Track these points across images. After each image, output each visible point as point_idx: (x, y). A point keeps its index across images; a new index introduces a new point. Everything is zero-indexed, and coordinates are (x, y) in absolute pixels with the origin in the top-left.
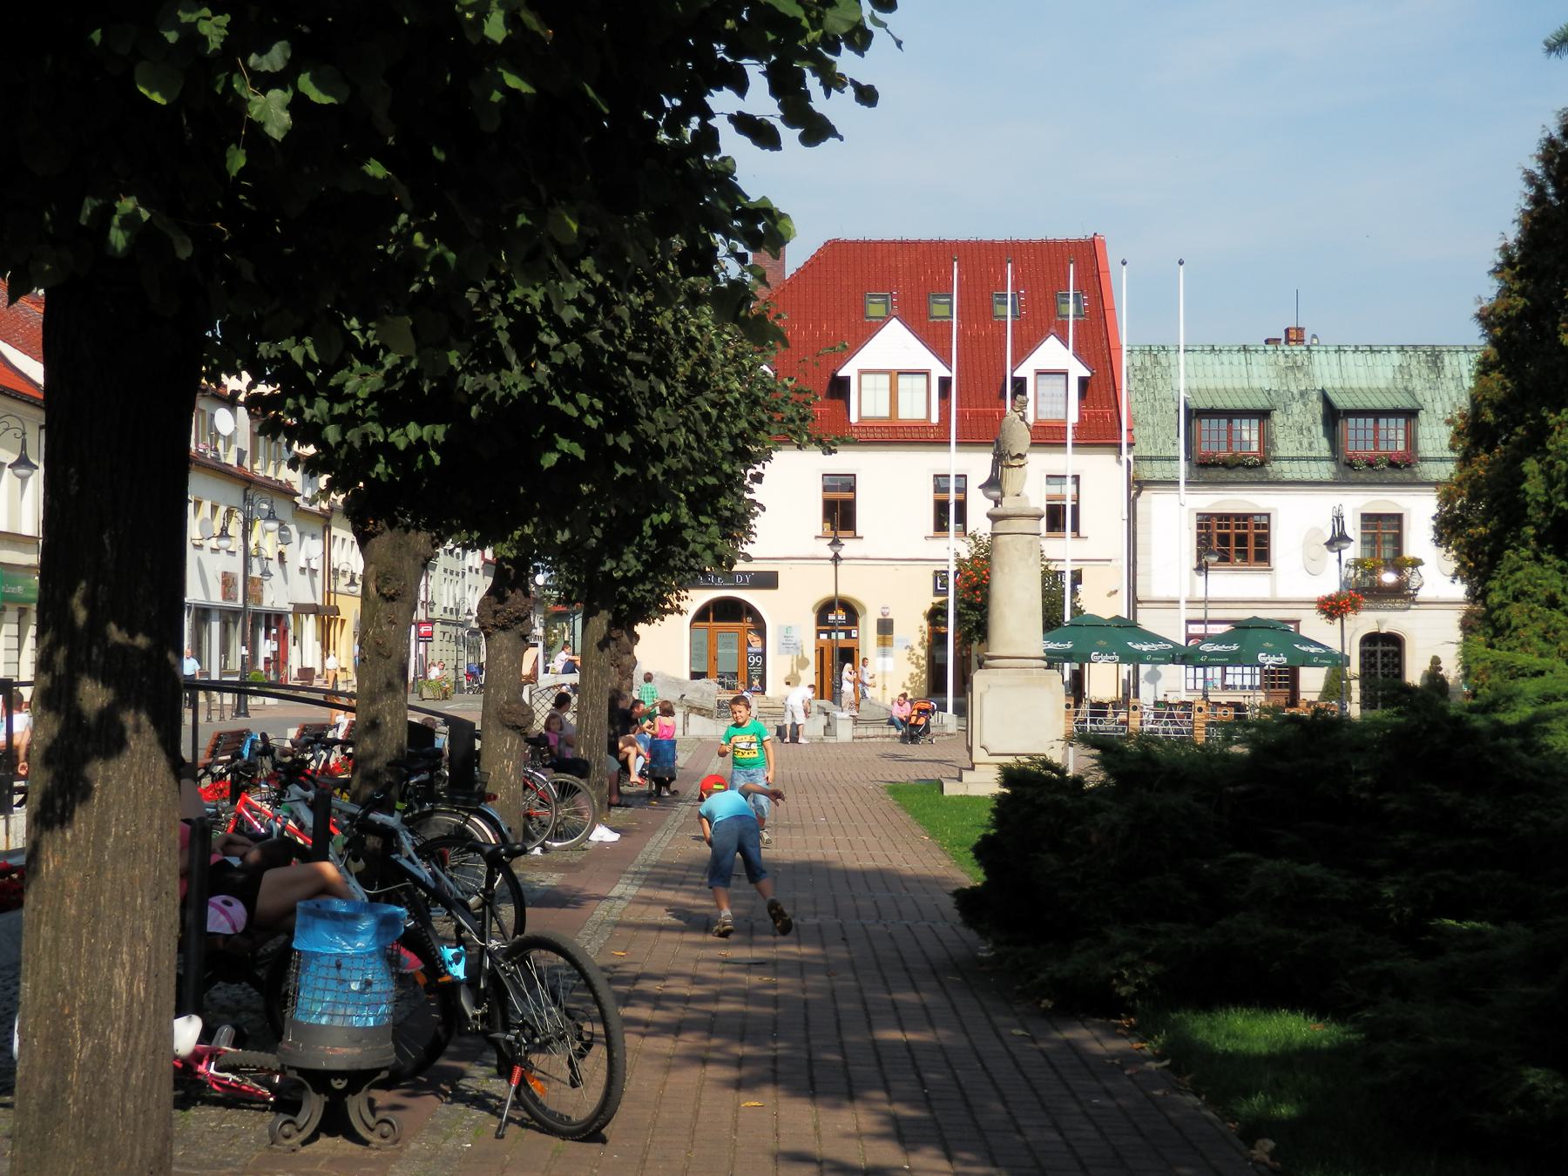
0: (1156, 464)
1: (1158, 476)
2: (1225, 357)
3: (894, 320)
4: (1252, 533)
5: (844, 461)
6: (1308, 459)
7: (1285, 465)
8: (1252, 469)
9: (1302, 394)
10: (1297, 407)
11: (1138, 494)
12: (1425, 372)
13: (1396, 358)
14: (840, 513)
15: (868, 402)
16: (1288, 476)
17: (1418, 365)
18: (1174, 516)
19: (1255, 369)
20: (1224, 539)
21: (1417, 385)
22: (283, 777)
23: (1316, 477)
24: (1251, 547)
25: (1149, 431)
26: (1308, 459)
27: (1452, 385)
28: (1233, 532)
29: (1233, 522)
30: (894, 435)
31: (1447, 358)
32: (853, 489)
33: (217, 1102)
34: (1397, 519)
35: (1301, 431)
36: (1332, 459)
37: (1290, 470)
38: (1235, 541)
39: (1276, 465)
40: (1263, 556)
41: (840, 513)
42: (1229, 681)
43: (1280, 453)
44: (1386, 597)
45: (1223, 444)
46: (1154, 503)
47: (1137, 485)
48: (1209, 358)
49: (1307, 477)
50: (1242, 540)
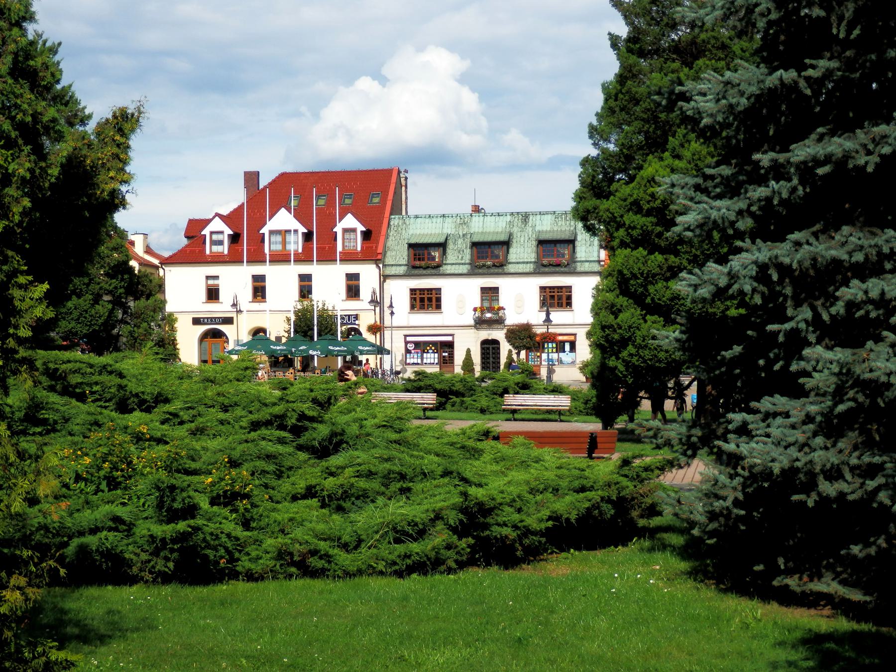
0: (394, 268)
1: (393, 273)
2: (434, 220)
3: (283, 209)
4: (434, 297)
5: (258, 270)
6: (459, 264)
7: (449, 267)
8: (435, 269)
9: (464, 235)
10: (460, 241)
11: (384, 281)
12: (520, 224)
13: (509, 218)
14: (259, 291)
15: (270, 246)
16: (448, 272)
17: (517, 221)
18: (399, 291)
19: (446, 225)
20: (422, 300)
21: (515, 230)
22: (844, 371)
23: (460, 272)
24: (564, 301)
25: (394, 253)
26: (459, 264)
27: (531, 229)
28: (426, 296)
29: (556, 290)
30: (281, 258)
31: (531, 217)
32: (264, 281)
33: (300, 499)
34: (569, 288)
35: (459, 252)
36: (470, 264)
37: (448, 269)
38: (426, 300)
39: (445, 267)
40: (569, 304)
41: (259, 291)
42: (425, 361)
43: (579, 259)
44: (485, 326)
45: (424, 256)
46: (390, 284)
47: (384, 278)
48: (427, 220)
49: (456, 272)
50: (430, 300)
